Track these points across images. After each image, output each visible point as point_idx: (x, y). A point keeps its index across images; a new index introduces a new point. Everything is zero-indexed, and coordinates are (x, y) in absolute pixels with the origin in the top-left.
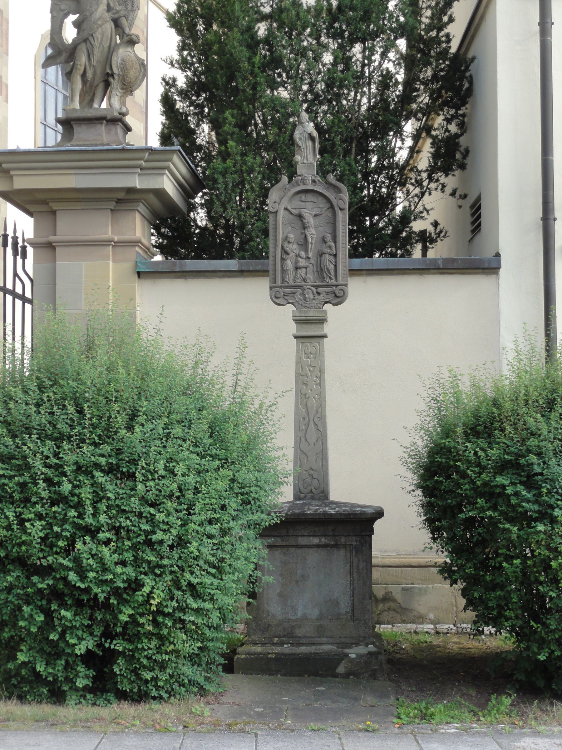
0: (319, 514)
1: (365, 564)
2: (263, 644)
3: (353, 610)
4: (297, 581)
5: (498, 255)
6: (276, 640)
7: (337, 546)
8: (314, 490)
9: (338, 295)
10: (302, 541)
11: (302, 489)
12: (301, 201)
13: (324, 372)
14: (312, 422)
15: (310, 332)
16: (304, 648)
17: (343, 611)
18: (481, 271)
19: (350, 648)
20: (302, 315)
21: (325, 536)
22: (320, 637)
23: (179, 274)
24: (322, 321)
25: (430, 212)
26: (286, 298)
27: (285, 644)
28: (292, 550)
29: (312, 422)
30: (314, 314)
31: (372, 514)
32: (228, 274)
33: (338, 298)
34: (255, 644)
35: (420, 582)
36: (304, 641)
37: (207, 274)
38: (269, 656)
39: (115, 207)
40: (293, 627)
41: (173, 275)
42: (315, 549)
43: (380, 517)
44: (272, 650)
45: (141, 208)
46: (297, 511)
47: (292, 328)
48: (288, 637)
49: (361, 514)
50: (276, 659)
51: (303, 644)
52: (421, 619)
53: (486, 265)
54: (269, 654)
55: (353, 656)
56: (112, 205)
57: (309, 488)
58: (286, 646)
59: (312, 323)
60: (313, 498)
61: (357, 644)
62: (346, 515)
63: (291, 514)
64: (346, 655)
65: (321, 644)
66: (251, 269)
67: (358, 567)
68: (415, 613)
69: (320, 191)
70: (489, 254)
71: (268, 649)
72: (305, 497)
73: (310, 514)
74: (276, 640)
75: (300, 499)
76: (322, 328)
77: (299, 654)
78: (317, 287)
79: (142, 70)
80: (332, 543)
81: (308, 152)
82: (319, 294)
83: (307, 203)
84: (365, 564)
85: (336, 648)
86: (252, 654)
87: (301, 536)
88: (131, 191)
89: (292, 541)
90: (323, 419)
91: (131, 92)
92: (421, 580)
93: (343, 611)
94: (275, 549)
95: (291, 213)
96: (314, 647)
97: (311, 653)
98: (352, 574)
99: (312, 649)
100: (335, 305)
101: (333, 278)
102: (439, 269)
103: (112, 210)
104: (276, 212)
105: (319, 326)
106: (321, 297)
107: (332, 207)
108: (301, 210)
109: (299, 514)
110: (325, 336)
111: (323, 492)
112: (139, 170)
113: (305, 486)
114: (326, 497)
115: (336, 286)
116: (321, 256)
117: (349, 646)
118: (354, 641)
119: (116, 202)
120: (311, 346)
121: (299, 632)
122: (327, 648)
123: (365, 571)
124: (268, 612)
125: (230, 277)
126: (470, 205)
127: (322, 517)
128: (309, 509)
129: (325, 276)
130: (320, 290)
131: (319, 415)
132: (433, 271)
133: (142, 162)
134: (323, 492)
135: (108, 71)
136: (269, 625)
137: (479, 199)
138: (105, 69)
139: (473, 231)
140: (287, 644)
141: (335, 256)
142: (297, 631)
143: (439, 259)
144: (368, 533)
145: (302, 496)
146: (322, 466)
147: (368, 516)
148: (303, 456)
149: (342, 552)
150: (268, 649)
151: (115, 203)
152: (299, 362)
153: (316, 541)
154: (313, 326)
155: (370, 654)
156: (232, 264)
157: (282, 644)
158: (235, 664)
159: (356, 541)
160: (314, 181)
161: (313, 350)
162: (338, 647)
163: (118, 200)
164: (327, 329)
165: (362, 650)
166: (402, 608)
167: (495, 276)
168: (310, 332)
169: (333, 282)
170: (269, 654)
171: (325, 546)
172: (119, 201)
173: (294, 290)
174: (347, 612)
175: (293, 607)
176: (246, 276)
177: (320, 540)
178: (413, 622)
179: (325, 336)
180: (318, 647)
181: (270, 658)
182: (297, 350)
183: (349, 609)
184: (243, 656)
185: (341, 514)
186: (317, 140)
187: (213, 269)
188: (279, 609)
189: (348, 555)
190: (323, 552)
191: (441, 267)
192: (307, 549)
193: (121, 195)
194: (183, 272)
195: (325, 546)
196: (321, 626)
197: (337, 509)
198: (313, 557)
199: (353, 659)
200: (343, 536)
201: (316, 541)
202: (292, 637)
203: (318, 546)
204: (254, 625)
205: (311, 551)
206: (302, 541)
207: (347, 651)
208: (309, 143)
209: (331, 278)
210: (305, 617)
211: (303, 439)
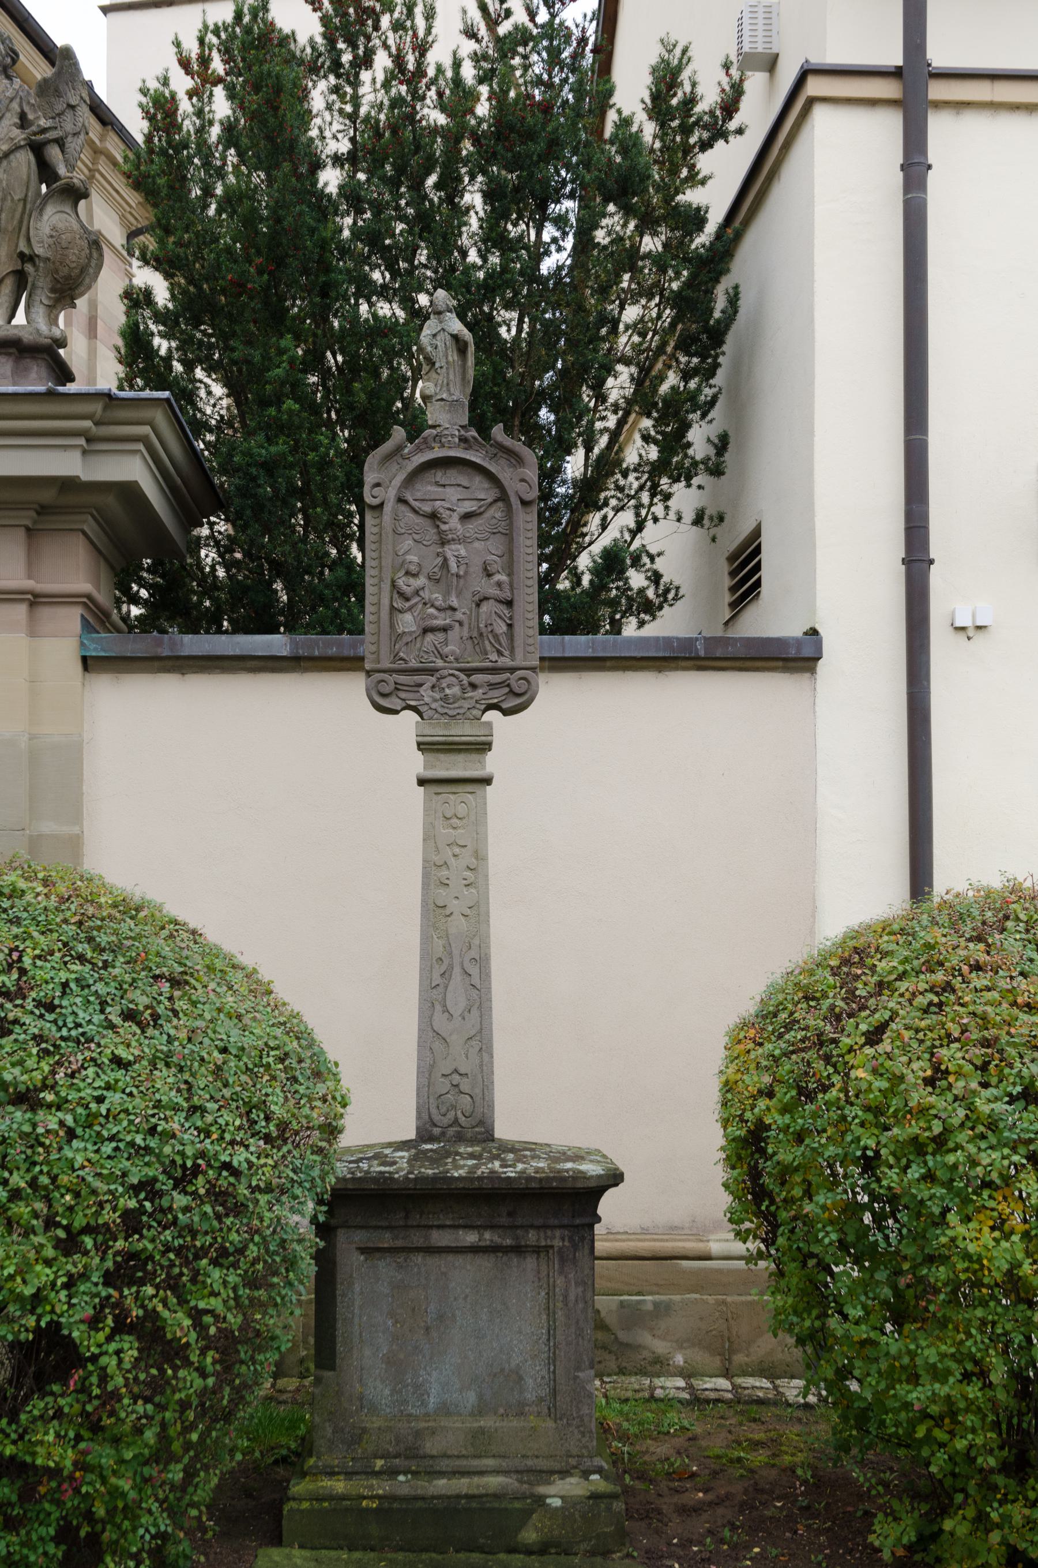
0: (480, 1179)
1: (580, 1289)
2: (349, 1475)
3: (554, 1392)
4: (427, 1329)
5: (814, 632)
6: (379, 1463)
7: (518, 1250)
8: (462, 1120)
9: (517, 690)
10: (440, 1238)
11: (437, 1118)
12: (437, 484)
13: (485, 859)
14: (457, 970)
15: (454, 770)
16: (442, 1482)
17: (530, 1396)
18: (780, 664)
19: (549, 1483)
20: (438, 732)
21: (492, 1227)
22: (479, 1457)
23: (170, 663)
24: (484, 747)
25: (657, 560)
26: (403, 695)
27: (398, 1473)
28: (419, 1258)
29: (457, 970)
30: (464, 731)
31: (599, 1176)
32: (270, 664)
33: (516, 701)
34: (331, 1474)
35: (655, 1289)
36: (444, 1464)
37: (226, 663)
38: (364, 1503)
39: (35, 522)
40: (418, 1434)
41: (156, 664)
42: (470, 1256)
43: (616, 1185)
44: (371, 1487)
45: (90, 526)
46: (430, 1172)
47: (417, 763)
48: (407, 1458)
49: (574, 1178)
50: (378, 1511)
51: (442, 1474)
52: (659, 1366)
53: (792, 653)
54: (365, 1498)
55: (556, 1502)
56: (27, 518)
57: (451, 1115)
58: (401, 1478)
59: (460, 751)
60: (460, 1138)
61: (564, 1473)
62: (541, 1180)
63: (416, 1179)
64: (540, 1500)
65: (482, 1473)
66: (317, 653)
67: (566, 1297)
68: (646, 1354)
69: (478, 461)
70: (793, 630)
71: (360, 1486)
72: (443, 1134)
73: (460, 1179)
74: (379, 1463)
75: (431, 1139)
76: (483, 764)
77: (433, 1497)
78: (469, 672)
79: (95, 255)
80: (508, 1242)
81: (451, 377)
82: (474, 686)
83: (448, 489)
84: (580, 1289)
85: (517, 1484)
86: (324, 1499)
87: (439, 1227)
88: (67, 485)
89: (417, 1239)
90: (482, 962)
91: (73, 298)
92: (657, 1285)
93: (530, 1396)
94: (378, 1255)
95: (415, 511)
96: (465, 1481)
97: (458, 1497)
98: (550, 1313)
99: (463, 1485)
100: (506, 712)
101: (506, 653)
102: (698, 658)
103: (28, 529)
104: (382, 504)
105: (474, 756)
106: (478, 693)
107: (503, 497)
108: (424, 530)
109: (435, 1179)
110: (487, 781)
111: (481, 1123)
112: (82, 441)
113: (443, 1110)
114: (489, 1136)
115: (513, 670)
116: (478, 605)
117: (546, 1475)
118: (557, 1466)
119: (38, 513)
120: (457, 801)
121: (430, 1446)
122: (494, 1482)
123: (581, 1305)
124: (361, 1398)
125: (273, 670)
126: (727, 554)
127: (487, 1185)
128: (457, 1167)
129: (489, 647)
130: (477, 678)
131: (473, 953)
132: (684, 664)
133: (88, 424)
134: (481, 1123)
135: (23, 247)
136: (364, 1430)
137: (757, 533)
138: (17, 245)
139: (733, 605)
140: (405, 1473)
141: (509, 604)
142: (428, 1445)
143: (697, 639)
144: (587, 1220)
145: (436, 1131)
146: (481, 1066)
147: (592, 1184)
148: (437, 1045)
149: (530, 1262)
150: (360, 1486)
151: (33, 514)
152: (429, 836)
153: (471, 1238)
154: (460, 758)
155: (595, 1496)
156: (277, 643)
157: (392, 1473)
158: (284, 1522)
159: (563, 1239)
160: (463, 440)
161: (462, 810)
162: (521, 1482)
163: (42, 507)
164: (492, 763)
165: (573, 1487)
166: (621, 1344)
167: (807, 675)
168: (454, 770)
169: (505, 661)
170: (365, 1498)
171: (493, 1249)
172: (43, 510)
173: (418, 679)
174: (541, 1399)
175: (417, 1387)
176: (306, 670)
177: (481, 1235)
178: (643, 1372)
179: (487, 781)
180: (476, 1480)
181: (368, 1510)
182: (426, 810)
183: (544, 1392)
184: (305, 1505)
185: (529, 1179)
186: (471, 348)
187: (238, 652)
188: (387, 1392)
189: (544, 1268)
190: (486, 1262)
191: (702, 654)
192: (450, 1257)
193: (47, 496)
194: (178, 658)
195: (493, 1249)
196: (482, 1431)
197: (520, 1166)
198: (464, 1275)
199: (556, 1509)
200: (532, 1226)
201: (471, 1238)
202: (416, 1457)
203: (474, 1250)
204: (329, 1430)
205: (459, 1260)
206: (440, 1238)
207: (542, 1490)
208: (453, 356)
209: (500, 653)
210: (445, 1410)
211: (438, 1008)
